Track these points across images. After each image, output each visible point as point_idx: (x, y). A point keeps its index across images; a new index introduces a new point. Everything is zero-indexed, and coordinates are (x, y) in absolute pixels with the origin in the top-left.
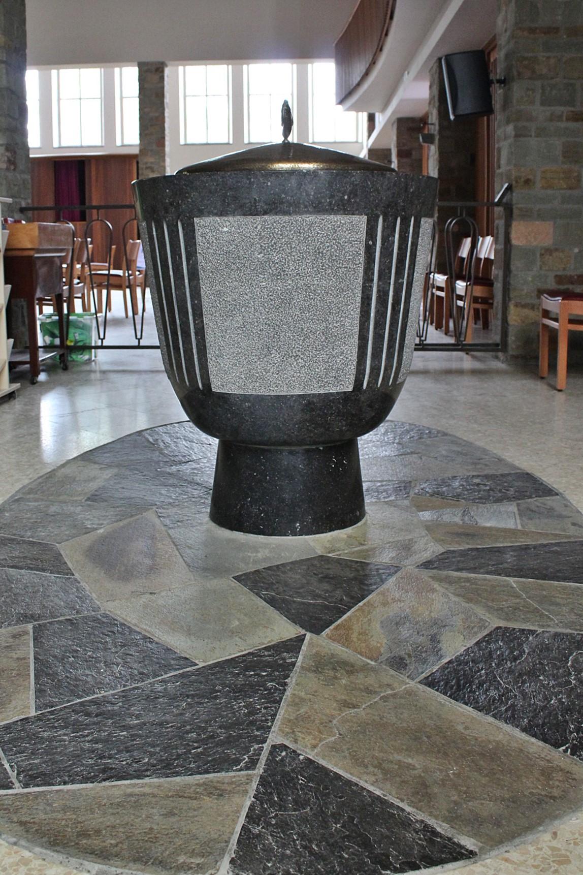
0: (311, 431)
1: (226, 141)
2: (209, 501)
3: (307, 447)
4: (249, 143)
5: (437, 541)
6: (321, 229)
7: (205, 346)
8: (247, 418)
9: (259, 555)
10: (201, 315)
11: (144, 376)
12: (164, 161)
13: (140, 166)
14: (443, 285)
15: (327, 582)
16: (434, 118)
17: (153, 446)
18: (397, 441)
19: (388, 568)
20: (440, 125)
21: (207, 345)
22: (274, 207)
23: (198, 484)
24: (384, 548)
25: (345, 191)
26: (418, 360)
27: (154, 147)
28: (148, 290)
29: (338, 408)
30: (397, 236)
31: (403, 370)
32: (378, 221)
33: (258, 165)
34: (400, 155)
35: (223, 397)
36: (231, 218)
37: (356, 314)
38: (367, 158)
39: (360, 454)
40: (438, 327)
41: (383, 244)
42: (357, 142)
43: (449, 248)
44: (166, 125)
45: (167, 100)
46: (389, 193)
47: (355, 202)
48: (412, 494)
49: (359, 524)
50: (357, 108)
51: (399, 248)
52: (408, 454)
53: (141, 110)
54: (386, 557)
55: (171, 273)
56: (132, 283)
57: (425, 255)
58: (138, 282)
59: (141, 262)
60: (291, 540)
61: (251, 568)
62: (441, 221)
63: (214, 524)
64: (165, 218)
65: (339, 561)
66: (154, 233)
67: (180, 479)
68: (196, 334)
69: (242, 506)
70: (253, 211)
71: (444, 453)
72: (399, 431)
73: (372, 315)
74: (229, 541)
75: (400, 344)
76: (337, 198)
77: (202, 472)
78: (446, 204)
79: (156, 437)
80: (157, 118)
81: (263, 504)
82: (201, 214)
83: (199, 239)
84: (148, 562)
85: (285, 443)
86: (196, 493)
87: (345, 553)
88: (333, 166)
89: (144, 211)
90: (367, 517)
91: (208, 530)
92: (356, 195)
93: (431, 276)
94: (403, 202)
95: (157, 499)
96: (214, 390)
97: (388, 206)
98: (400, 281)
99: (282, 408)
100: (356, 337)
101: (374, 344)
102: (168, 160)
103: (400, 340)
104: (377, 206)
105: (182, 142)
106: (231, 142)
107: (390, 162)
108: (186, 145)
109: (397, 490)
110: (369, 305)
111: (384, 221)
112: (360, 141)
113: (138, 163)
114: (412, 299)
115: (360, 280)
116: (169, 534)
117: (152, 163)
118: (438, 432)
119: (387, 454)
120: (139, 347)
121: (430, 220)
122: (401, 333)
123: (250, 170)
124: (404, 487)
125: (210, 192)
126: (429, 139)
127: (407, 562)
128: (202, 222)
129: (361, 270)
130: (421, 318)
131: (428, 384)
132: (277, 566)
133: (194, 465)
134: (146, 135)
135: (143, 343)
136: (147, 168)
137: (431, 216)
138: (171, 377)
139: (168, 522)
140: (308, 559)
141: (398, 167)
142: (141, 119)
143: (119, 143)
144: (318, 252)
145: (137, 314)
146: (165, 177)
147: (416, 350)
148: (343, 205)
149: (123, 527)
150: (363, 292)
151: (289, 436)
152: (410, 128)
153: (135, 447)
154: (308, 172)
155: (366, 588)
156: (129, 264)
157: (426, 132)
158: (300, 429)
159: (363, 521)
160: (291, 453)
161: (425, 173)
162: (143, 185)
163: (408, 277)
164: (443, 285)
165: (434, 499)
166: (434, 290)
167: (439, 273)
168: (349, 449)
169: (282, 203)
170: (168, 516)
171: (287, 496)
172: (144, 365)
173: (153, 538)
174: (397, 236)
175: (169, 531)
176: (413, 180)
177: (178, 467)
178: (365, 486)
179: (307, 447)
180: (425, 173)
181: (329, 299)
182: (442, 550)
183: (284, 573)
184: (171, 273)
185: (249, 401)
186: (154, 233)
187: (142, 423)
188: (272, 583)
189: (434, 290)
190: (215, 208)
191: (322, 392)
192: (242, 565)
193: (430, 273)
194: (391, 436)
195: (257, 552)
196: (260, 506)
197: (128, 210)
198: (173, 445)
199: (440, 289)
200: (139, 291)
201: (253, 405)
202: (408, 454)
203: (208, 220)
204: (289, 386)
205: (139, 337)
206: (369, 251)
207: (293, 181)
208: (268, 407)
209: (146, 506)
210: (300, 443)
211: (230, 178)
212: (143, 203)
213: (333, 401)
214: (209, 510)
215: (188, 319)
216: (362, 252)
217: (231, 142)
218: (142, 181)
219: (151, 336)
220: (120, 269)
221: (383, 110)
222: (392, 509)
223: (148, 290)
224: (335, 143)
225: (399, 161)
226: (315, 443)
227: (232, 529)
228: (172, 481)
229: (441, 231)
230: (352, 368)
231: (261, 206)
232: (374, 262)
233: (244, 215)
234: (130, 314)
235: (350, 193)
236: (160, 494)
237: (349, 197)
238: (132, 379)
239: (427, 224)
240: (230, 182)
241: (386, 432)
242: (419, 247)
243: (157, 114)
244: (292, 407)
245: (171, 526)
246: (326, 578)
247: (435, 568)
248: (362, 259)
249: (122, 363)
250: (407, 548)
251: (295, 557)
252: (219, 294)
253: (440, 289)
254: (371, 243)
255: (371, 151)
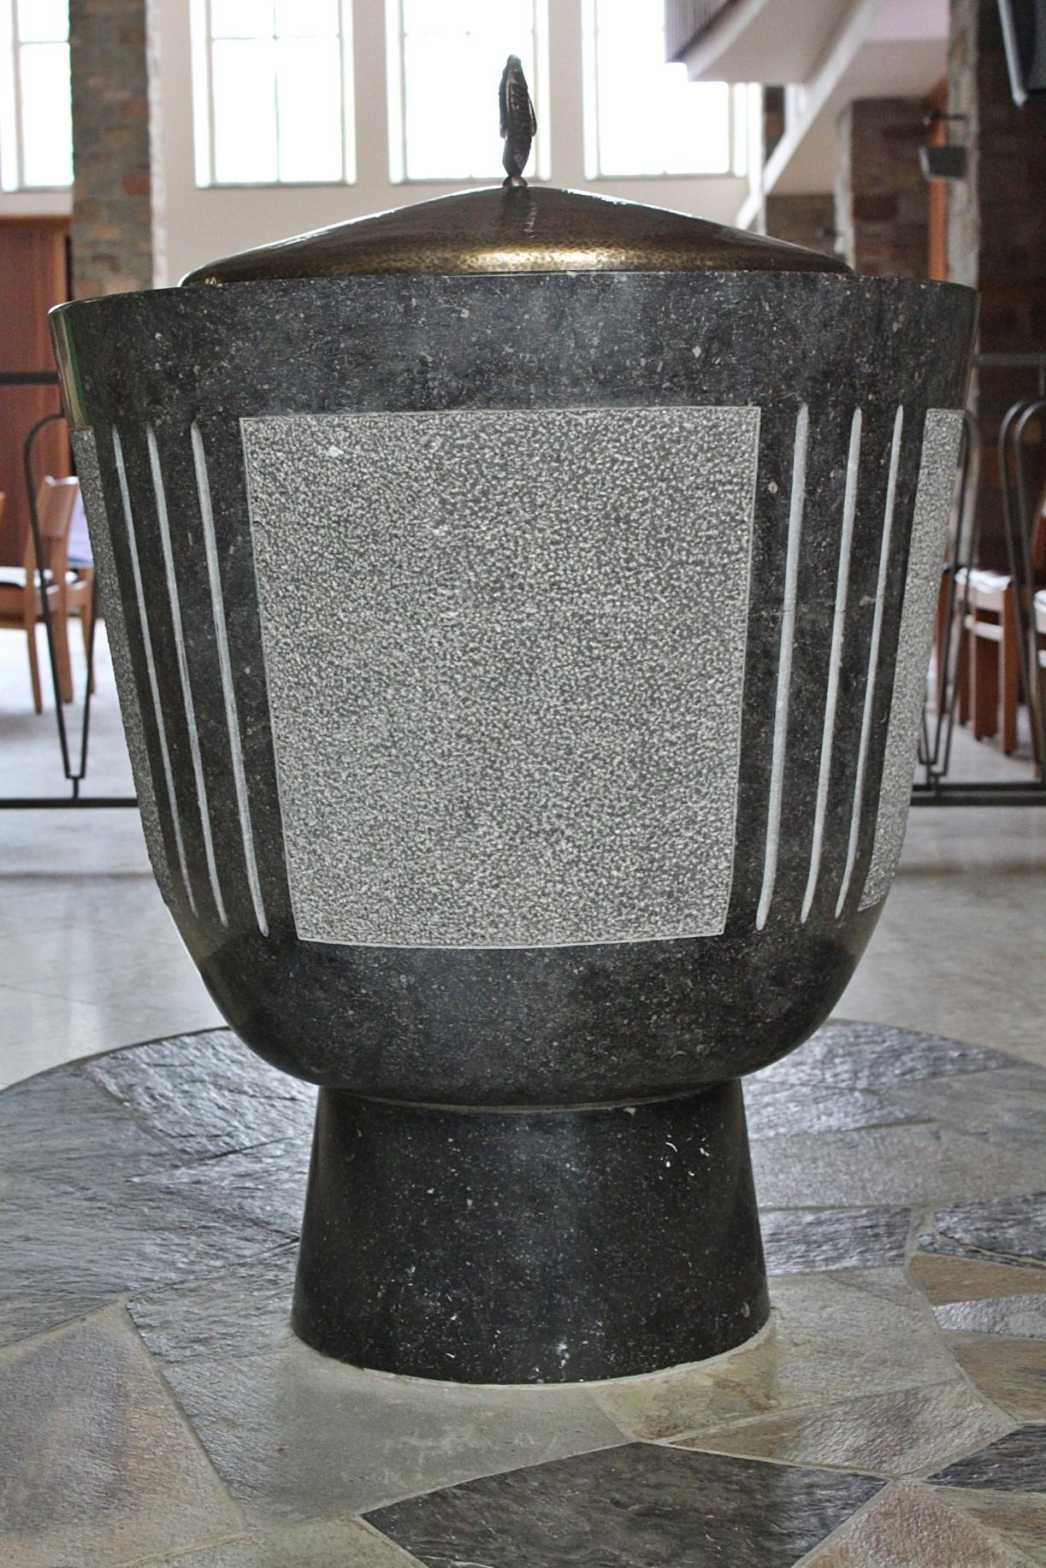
0: (598, 1057)
1: (335, 177)
2: (290, 1276)
3: (588, 1107)
4: (407, 183)
5: (991, 1393)
6: (623, 449)
7: (275, 805)
8: (404, 1021)
9: (446, 1443)
10: (263, 710)
11: (92, 891)
12: (148, 235)
13: (77, 252)
14: (997, 605)
15: (656, 1527)
16: (964, 99)
17: (118, 1107)
18: (862, 1084)
19: (842, 1482)
20: (982, 119)
21: (283, 801)
22: (481, 382)
23: (256, 1222)
24: (829, 1418)
25: (695, 333)
26: (924, 833)
27: (118, 194)
28: (101, 629)
29: (681, 987)
30: (852, 466)
31: (876, 870)
32: (794, 420)
33: (431, 257)
34: (863, 210)
35: (332, 959)
36: (351, 419)
37: (731, 703)
38: (762, 232)
39: (752, 1121)
40: (984, 731)
41: (810, 490)
42: (730, 175)
43: (1012, 491)
44: (155, 129)
45: (155, 51)
46: (826, 336)
47: (726, 365)
48: (911, 1249)
49: (751, 1343)
50: (729, 70)
51: (861, 503)
52: (897, 1123)
53: (75, 79)
54: (834, 1449)
55: (172, 584)
56: (53, 606)
57: (941, 511)
58: (72, 607)
59: (79, 544)
60: (542, 1395)
61: (422, 1487)
62: (991, 408)
63: (304, 1348)
64: (151, 417)
65: (688, 1461)
66: (120, 464)
67: (203, 1206)
68: (249, 768)
69: (392, 1292)
70: (416, 396)
71: (1007, 1119)
72: (869, 1053)
73: (781, 704)
74: (351, 1401)
75: (865, 792)
76: (668, 355)
77: (270, 1186)
78: (1004, 360)
79: (128, 1078)
80: (125, 106)
81: (456, 1285)
82: (260, 404)
83: (255, 482)
84: (102, 1471)
85: (520, 1096)
86: (249, 1250)
87: (710, 1436)
88: (658, 257)
89: (87, 397)
90: (775, 1321)
91: (287, 1368)
92: (729, 345)
93: (960, 578)
94: (872, 361)
95: (130, 1272)
96: (302, 936)
97: (827, 375)
98: (866, 599)
99: (509, 990)
100: (734, 770)
101: (786, 792)
102: (160, 234)
103: (866, 780)
104: (789, 378)
105: (203, 180)
106: (351, 178)
107: (831, 233)
108: (214, 187)
109: (865, 1237)
110: (771, 674)
111: (813, 421)
112: (739, 171)
113: (68, 242)
114: (900, 655)
115: (743, 602)
116: (166, 1382)
117: (112, 243)
118: (990, 1055)
119: (834, 1123)
120: (75, 802)
121: (954, 417)
122: (869, 758)
123: (407, 273)
124: (888, 1226)
125: (289, 340)
126: (950, 162)
127: (901, 1464)
128: (264, 431)
129: (746, 569)
130: (932, 704)
131: (955, 907)
132: (502, 1479)
133: (245, 1165)
134: (94, 157)
135: (87, 790)
136: (97, 258)
137: (956, 403)
138: (173, 895)
139: (162, 1342)
140: (597, 1456)
141: (859, 249)
142: (77, 108)
143: (10, 184)
144: (616, 518)
145: (69, 700)
146: (152, 296)
147: (915, 802)
148: (689, 375)
149: (25, 1362)
150: (752, 637)
151: (533, 1074)
152: (890, 127)
153: (62, 1111)
154: (583, 278)
155: (775, 1546)
156: (46, 552)
157: (940, 140)
158: (565, 1054)
159: (764, 1332)
160: (538, 1124)
161: (937, 275)
162: (77, 313)
163: (888, 587)
164: (997, 605)
165: (979, 1263)
166: (970, 621)
167: (984, 566)
168: (712, 1111)
169: (503, 370)
170: (165, 1325)
171: (528, 1258)
172: (92, 858)
173: (117, 1394)
174: (852, 466)
175: (174, 1374)
176: (898, 294)
177: (197, 1172)
178: (767, 1224)
179: (588, 1107)
180: (937, 275)
181: (648, 658)
182: (1009, 1425)
183: (521, 1499)
184: (172, 584)
185: (409, 970)
186: (120, 464)
187: (85, 1034)
188: (487, 1535)
189: (970, 621)
190: (304, 388)
191: (631, 939)
192: (391, 1477)
193: (957, 568)
194: (843, 1067)
195: (440, 1434)
196: (445, 1290)
197: (41, 389)
198: (179, 1102)
199: (987, 616)
200: (75, 630)
201: (422, 980)
202: (897, 1123)
203: (281, 424)
204: (531, 922)
205: (75, 771)
206: (770, 512)
207: (537, 307)
208: (469, 987)
209: (95, 1296)
210: (568, 1095)
211: (348, 296)
212: (82, 373)
213: (664, 967)
214: (289, 1304)
215: (224, 723)
216: (748, 514)
217: (351, 178)
218: (81, 305)
219: (113, 767)
220: (15, 562)
221: (809, 76)
222: (852, 1295)
223: (101, 629)
224: (665, 178)
225: (859, 235)
226: (611, 1095)
227: (361, 1361)
228: (176, 1214)
229: (989, 442)
230: (723, 865)
231: (440, 380)
232: (785, 546)
233: (391, 407)
234: (49, 699)
235: (710, 339)
236: (142, 1255)
237: (706, 351)
238: (57, 900)
239: (943, 428)
240: (347, 309)
241: (830, 1056)
242: (920, 498)
243: (125, 95)
244: (540, 987)
245: (174, 1355)
246: (653, 1516)
247: (989, 1483)
248: (747, 539)
249: (25, 852)
250: (901, 1418)
251: (555, 1450)
252: (317, 645)
253: (987, 616)
254: (773, 487)
255: (774, 203)
